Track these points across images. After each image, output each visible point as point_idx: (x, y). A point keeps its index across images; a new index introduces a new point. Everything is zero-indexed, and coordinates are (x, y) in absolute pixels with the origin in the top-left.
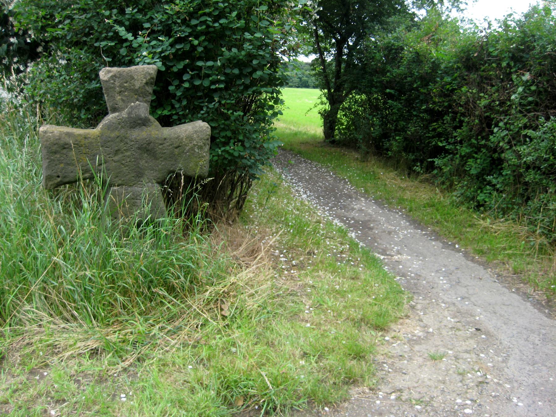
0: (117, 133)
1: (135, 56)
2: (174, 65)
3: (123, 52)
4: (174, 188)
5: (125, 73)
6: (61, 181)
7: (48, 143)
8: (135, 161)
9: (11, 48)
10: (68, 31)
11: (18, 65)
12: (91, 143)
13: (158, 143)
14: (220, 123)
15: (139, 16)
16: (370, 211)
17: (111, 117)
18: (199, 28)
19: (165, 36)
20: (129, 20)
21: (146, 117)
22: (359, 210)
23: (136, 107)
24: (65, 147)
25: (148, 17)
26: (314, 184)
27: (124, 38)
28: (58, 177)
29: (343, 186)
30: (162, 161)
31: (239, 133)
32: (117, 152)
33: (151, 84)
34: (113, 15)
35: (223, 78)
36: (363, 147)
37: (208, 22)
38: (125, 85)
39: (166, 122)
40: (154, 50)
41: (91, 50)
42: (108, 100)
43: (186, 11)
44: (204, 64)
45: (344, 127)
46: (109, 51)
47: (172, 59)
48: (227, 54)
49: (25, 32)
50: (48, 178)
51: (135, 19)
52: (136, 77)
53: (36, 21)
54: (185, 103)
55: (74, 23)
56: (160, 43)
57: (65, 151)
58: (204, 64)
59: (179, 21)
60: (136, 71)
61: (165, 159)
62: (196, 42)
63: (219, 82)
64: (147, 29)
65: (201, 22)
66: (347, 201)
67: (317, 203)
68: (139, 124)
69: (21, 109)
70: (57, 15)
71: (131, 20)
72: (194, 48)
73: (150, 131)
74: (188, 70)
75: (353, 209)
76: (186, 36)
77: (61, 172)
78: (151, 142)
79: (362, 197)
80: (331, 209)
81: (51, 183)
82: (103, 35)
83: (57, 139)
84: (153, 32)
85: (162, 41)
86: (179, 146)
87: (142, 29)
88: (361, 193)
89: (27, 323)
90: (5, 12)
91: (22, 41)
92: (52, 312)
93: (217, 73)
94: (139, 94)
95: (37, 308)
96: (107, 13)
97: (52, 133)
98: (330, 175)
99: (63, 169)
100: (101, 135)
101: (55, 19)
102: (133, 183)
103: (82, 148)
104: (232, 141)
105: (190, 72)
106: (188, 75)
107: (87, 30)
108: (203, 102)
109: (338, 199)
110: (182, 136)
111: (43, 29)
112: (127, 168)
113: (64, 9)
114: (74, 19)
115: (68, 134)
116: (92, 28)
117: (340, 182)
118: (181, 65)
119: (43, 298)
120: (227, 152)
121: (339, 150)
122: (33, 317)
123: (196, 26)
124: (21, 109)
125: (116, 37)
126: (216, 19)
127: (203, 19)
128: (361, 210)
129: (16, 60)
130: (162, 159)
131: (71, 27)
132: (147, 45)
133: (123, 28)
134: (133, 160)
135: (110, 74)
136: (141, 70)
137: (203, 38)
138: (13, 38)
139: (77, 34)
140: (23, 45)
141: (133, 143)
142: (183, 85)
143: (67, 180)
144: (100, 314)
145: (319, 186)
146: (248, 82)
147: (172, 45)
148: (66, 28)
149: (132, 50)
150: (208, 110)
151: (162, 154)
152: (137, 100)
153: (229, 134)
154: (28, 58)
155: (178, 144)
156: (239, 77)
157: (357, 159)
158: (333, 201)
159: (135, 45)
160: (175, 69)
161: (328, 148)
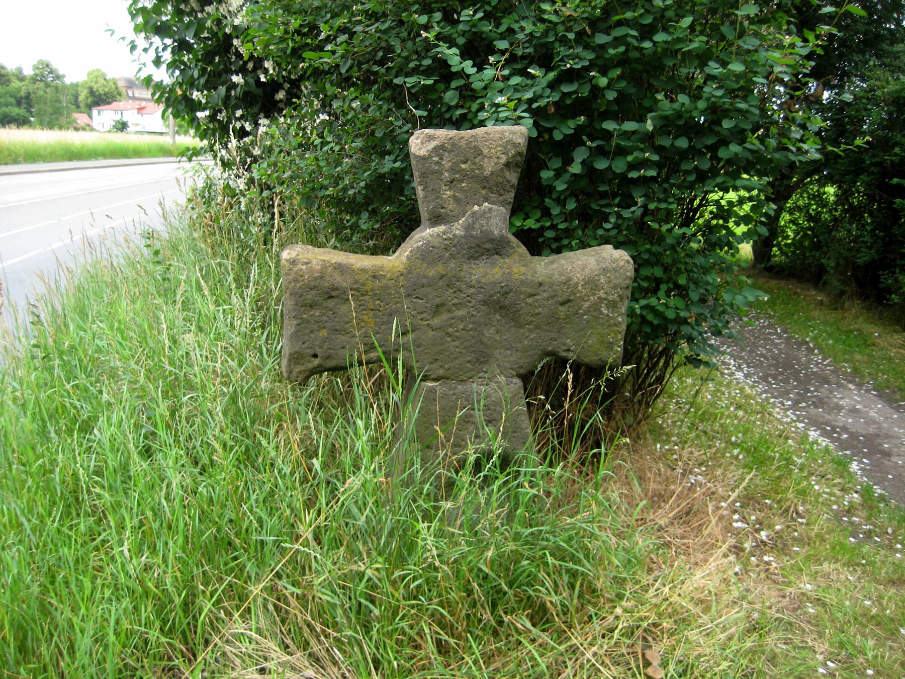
0: (440, 269)
1: (475, 106)
2: (555, 128)
3: (451, 97)
4: (545, 380)
5: (463, 142)
6: (320, 366)
7: (298, 285)
8: (474, 329)
9: (233, 93)
10: (342, 57)
11: (243, 122)
12: (386, 287)
13: (525, 293)
14: (642, 249)
15: (487, 27)
16: (872, 414)
17: (424, 234)
18: (612, 51)
19: (540, 66)
20: (464, 34)
21: (502, 236)
22: (850, 411)
23: (483, 214)
24: (333, 294)
25: (502, 28)
26: (751, 352)
27: (454, 70)
28: (315, 356)
29: (806, 356)
30: (530, 331)
31: (679, 271)
32: (438, 309)
33: (517, 165)
34: (435, 25)
35: (655, 158)
36: (835, 283)
37: (629, 39)
38: (463, 166)
39: (535, 243)
40: (518, 95)
41: (388, 94)
42: (425, 197)
43: (585, 15)
44: (617, 127)
45: (789, 241)
46: (423, 96)
47: (553, 114)
48: (665, 106)
49: (259, 63)
50: (296, 358)
51: (475, 33)
52: (485, 151)
53: (282, 40)
54: (571, 205)
55: (355, 41)
56: (529, 82)
57: (331, 303)
58: (617, 127)
59: (571, 36)
60: (487, 138)
61: (537, 327)
62: (603, 82)
63: (643, 164)
64: (503, 52)
65: (616, 39)
66: (822, 390)
67: (765, 392)
68: (488, 250)
69: (242, 199)
70: (322, 26)
71: (467, 35)
72: (596, 91)
73: (510, 267)
74: (584, 138)
75: (839, 408)
76: (583, 68)
77: (321, 347)
78: (511, 291)
79: (850, 382)
80: (795, 406)
81: (298, 368)
82: (412, 65)
83: (316, 278)
84: (513, 59)
85: (533, 77)
86: (569, 301)
87: (493, 52)
88: (845, 373)
89: (238, 661)
90: (227, 31)
91: (252, 81)
92: (289, 641)
93: (642, 146)
94: (489, 186)
95: (259, 631)
96: (423, 19)
97: (307, 263)
98: (776, 333)
99: (325, 340)
100: (409, 271)
101: (319, 34)
102: (468, 375)
103: (367, 298)
104: (664, 287)
105: (589, 143)
106: (583, 148)
107: (380, 54)
108: (609, 205)
109: (803, 384)
110: (576, 280)
111: (297, 53)
112: (457, 343)
113: (335, 15)
114: (355, 32)
115: (340, 268)
116: (389, 49)
117: (799, 349)
118: (569, 127)
119: (271, 607)
120: (652, 309)
121: (783, 283)
122: (250, 652)
123: (603, 47)
124: (242, 199)
125: (442, 64)
126: (647, 32)
127: (619, 32)
128: (853, 411)
129: (239, 113)
130: (531, 327)
131: (350, 48)
132: (500, 85)
133: (454, 50)
134: (471, 326)
135: (433, 144)
136: (498, 135)
137: (616, 72)
138: (238, 75)
139: (360, 64)
140: (253, 87)
141: (472, 290)
142: (570, 169)
143: (331, 363)
144: (389, 662)
145: (762, 355)
146: (705, 165)
147: (552, 86)
148: (340, 51)
149: (468, 94)
150: (620, 222)
151: (532, 316)
152: (486, 199)
153: (658, 272)
154: (260, 111)
155: (567, 298)
156: (692, 152)
157: (821, 303)
158: (795, 388)
159: (477, 85)
160: (558, 136)
161: (764, 280)
